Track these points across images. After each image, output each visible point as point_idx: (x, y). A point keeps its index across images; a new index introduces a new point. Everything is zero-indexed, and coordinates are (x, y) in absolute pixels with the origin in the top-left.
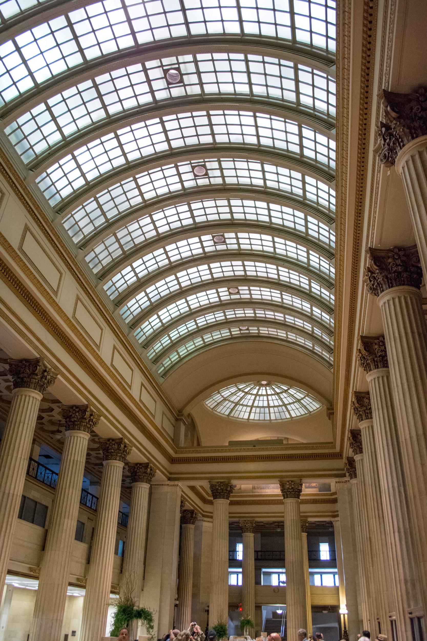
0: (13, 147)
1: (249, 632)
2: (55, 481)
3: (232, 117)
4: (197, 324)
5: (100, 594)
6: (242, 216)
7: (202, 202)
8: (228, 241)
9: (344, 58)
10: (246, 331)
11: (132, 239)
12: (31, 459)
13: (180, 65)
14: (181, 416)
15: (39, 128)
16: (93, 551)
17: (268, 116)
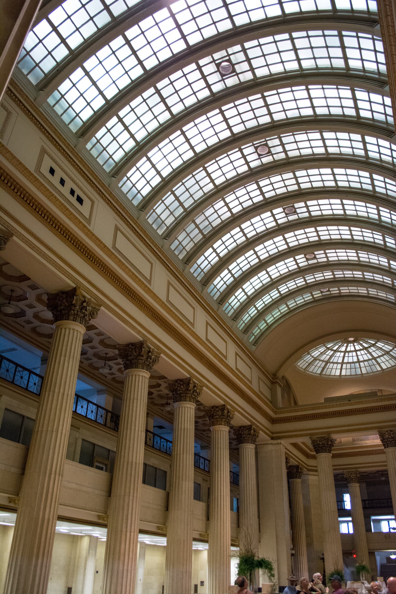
0: (95, 159)
1: (366, 578)
2: (170, 448)
3: (286, 94)
4: (279, 292)
5: (222, 547)
6: (308, 185)
7: (269, 178)
8: (298, 211)
9: (387, 16)
10: (327, 293)
11: (210, 223)
12: (147, 431)
13: (231, 56)
14: (274, 379)
15: (115, 139)
16: (211, 511)
17: (320, 87)
